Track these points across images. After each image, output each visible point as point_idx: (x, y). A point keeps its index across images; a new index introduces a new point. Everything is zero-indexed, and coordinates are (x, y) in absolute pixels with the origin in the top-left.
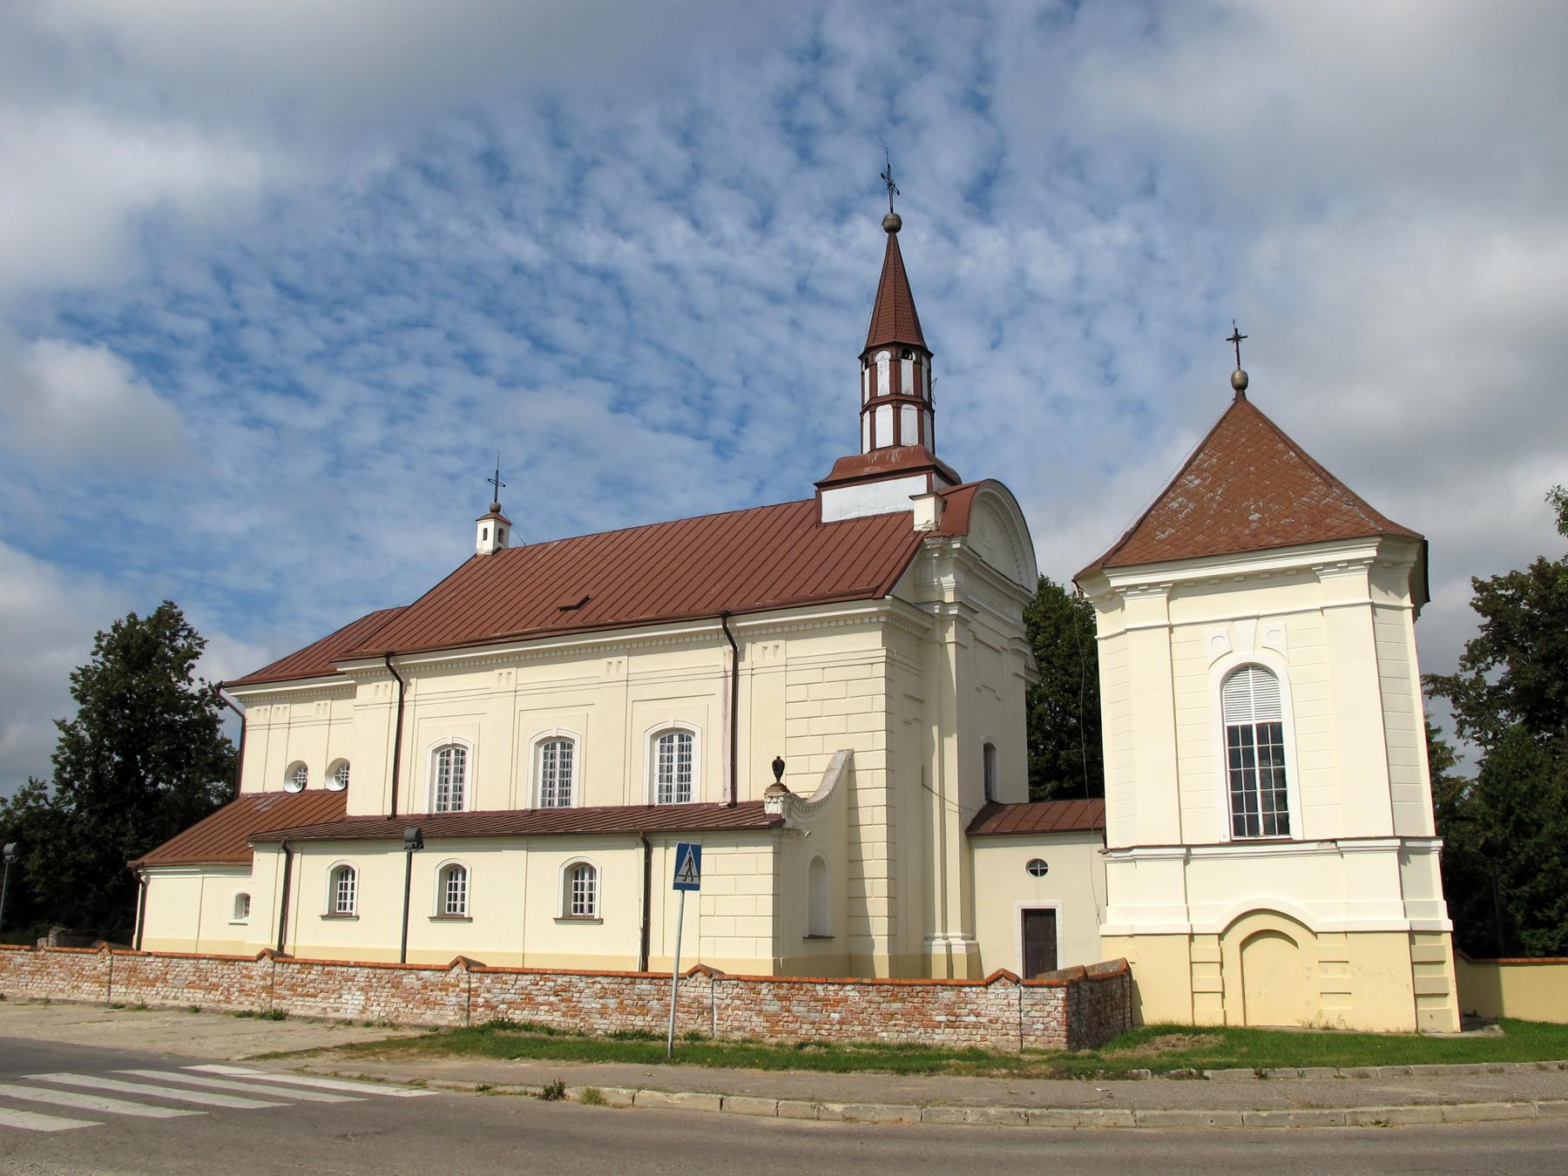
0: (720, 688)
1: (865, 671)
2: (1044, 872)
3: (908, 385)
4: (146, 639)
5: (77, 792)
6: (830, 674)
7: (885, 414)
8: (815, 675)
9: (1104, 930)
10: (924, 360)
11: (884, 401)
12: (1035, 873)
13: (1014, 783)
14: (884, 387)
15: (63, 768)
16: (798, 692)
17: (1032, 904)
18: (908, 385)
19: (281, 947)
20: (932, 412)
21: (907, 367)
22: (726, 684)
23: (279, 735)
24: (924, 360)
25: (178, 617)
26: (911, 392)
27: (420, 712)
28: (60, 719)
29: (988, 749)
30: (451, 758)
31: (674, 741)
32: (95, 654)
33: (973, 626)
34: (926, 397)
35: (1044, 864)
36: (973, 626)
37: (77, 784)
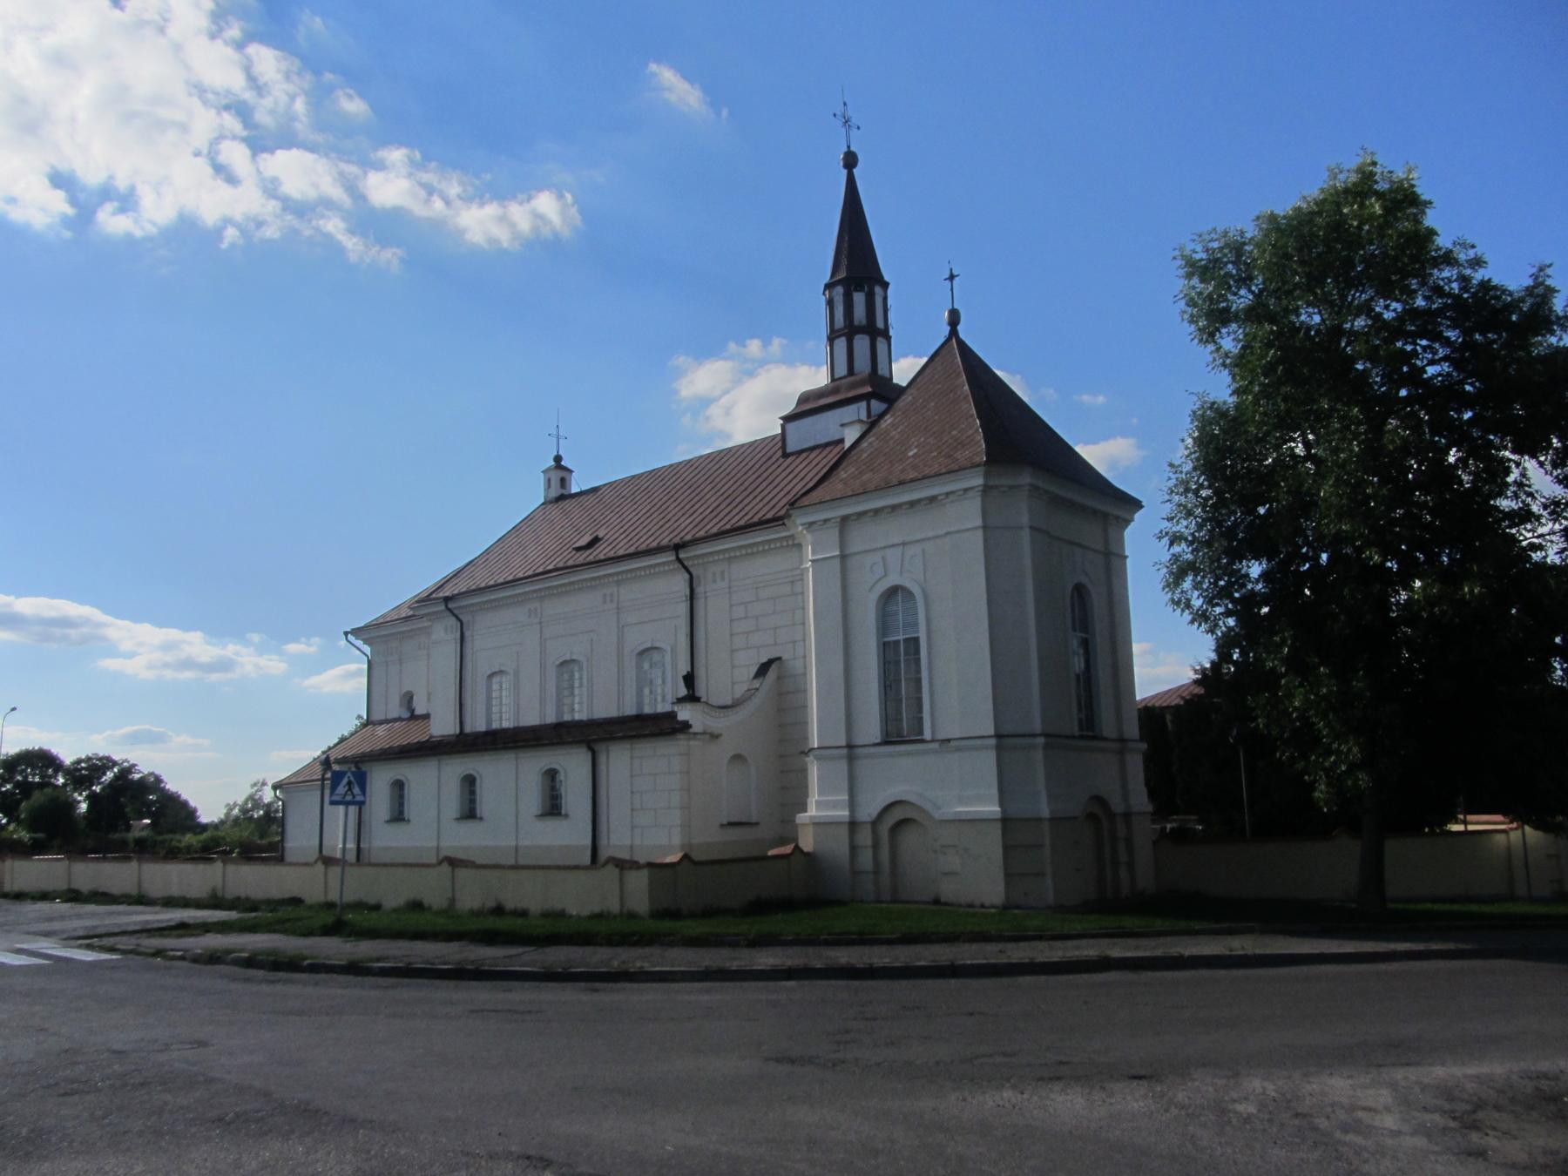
0: (683, 608)
21: (859, 299)
24: (878, 290)
26: (864, 322)
34: (880, 324)
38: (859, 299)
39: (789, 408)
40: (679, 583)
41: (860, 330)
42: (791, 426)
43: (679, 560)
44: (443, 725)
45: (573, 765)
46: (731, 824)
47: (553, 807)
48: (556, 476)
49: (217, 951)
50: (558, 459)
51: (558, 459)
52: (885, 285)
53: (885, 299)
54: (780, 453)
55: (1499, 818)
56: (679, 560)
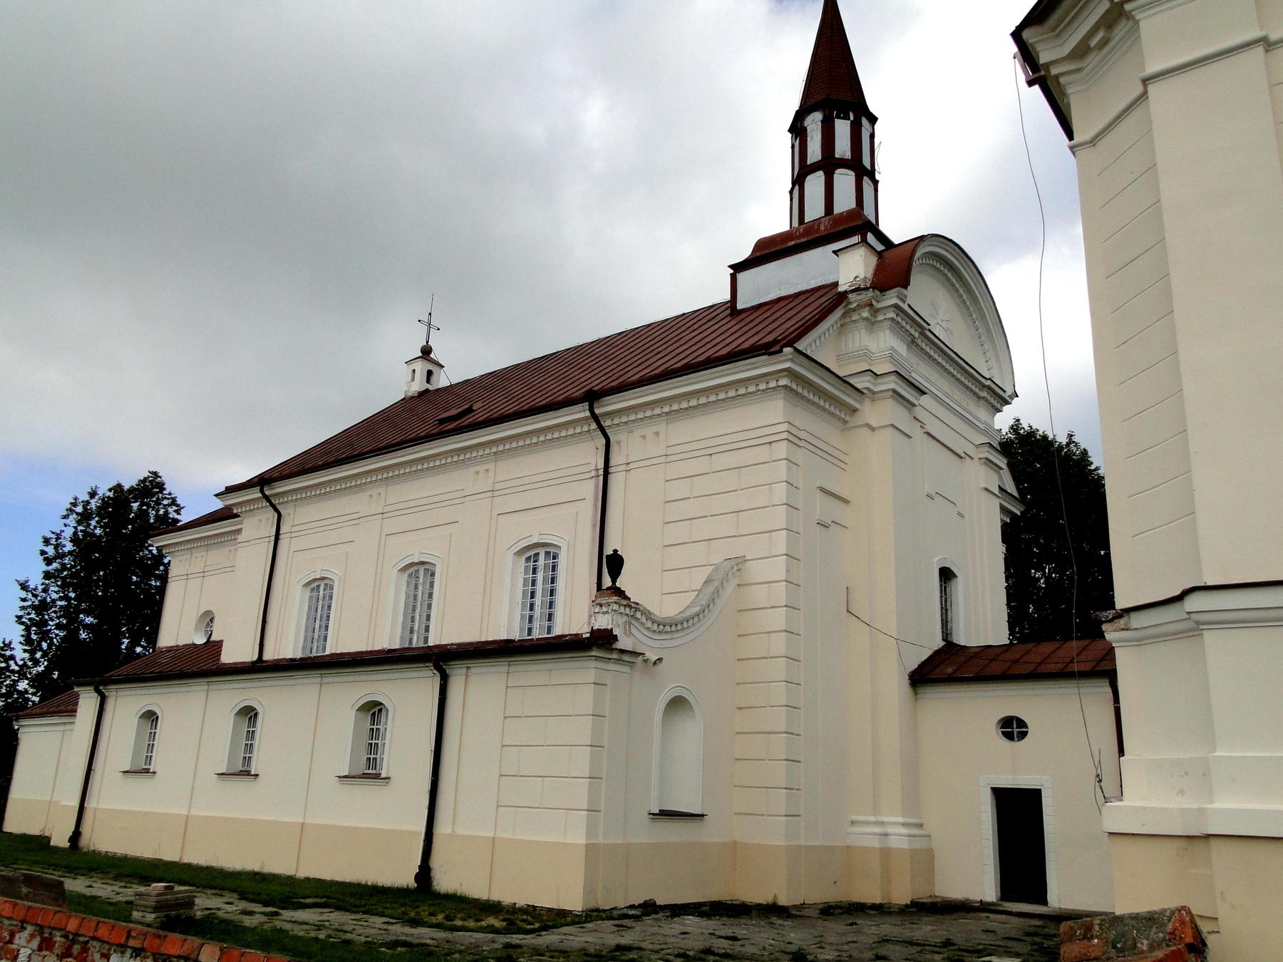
0: (590, 490)
1: (762, 454)
2: (1023, 735)
3: (843, 147)
4: (914, 853)
5: (45, 654)
6: (720, 462)
7: (815, 183)
8: (700, 465)
9: (1118, 817)
10: (864, 121)
11: (814, 168)
12: (1009, 736)
13: (985, 620)
14: (815, 152)
15: (28, 629)
16: (681, 489)
17: (1007, 782)
18: (843, 147)
19: (424, 873)
20: (876, 183)
21: (842, 128)
22: (597, 487)
23: (194, 584)
24: (864, 121)
25: (161, 487)
26: (848, 155)
27: (298, 543)
28: (22, 580)
29: (946, 575)
30: (320, 589)
31: (540, 559)
32: (65, 517)
33: (919, 412)
34: (866, 162)
35: (1022, 724)
36: (919, 412)
37: (45, 645)
38: (842, 128)
39: (745, 253)
40: (588, 454)
41: (843, 164)
42: (741, 277)
43: (595, 417)
44: (237, 650)
45: (410, 697)
46: (665, 814)
47: (369, 772)
48: (421, 367)
49: (1155, 912)
50: (426, 351)
51: (426, 351)
52: (873, 119)
53: (872, 136)
54: (728, 312)
55: (299, 931)
56: (595, 417)
